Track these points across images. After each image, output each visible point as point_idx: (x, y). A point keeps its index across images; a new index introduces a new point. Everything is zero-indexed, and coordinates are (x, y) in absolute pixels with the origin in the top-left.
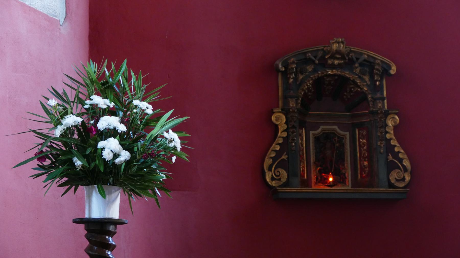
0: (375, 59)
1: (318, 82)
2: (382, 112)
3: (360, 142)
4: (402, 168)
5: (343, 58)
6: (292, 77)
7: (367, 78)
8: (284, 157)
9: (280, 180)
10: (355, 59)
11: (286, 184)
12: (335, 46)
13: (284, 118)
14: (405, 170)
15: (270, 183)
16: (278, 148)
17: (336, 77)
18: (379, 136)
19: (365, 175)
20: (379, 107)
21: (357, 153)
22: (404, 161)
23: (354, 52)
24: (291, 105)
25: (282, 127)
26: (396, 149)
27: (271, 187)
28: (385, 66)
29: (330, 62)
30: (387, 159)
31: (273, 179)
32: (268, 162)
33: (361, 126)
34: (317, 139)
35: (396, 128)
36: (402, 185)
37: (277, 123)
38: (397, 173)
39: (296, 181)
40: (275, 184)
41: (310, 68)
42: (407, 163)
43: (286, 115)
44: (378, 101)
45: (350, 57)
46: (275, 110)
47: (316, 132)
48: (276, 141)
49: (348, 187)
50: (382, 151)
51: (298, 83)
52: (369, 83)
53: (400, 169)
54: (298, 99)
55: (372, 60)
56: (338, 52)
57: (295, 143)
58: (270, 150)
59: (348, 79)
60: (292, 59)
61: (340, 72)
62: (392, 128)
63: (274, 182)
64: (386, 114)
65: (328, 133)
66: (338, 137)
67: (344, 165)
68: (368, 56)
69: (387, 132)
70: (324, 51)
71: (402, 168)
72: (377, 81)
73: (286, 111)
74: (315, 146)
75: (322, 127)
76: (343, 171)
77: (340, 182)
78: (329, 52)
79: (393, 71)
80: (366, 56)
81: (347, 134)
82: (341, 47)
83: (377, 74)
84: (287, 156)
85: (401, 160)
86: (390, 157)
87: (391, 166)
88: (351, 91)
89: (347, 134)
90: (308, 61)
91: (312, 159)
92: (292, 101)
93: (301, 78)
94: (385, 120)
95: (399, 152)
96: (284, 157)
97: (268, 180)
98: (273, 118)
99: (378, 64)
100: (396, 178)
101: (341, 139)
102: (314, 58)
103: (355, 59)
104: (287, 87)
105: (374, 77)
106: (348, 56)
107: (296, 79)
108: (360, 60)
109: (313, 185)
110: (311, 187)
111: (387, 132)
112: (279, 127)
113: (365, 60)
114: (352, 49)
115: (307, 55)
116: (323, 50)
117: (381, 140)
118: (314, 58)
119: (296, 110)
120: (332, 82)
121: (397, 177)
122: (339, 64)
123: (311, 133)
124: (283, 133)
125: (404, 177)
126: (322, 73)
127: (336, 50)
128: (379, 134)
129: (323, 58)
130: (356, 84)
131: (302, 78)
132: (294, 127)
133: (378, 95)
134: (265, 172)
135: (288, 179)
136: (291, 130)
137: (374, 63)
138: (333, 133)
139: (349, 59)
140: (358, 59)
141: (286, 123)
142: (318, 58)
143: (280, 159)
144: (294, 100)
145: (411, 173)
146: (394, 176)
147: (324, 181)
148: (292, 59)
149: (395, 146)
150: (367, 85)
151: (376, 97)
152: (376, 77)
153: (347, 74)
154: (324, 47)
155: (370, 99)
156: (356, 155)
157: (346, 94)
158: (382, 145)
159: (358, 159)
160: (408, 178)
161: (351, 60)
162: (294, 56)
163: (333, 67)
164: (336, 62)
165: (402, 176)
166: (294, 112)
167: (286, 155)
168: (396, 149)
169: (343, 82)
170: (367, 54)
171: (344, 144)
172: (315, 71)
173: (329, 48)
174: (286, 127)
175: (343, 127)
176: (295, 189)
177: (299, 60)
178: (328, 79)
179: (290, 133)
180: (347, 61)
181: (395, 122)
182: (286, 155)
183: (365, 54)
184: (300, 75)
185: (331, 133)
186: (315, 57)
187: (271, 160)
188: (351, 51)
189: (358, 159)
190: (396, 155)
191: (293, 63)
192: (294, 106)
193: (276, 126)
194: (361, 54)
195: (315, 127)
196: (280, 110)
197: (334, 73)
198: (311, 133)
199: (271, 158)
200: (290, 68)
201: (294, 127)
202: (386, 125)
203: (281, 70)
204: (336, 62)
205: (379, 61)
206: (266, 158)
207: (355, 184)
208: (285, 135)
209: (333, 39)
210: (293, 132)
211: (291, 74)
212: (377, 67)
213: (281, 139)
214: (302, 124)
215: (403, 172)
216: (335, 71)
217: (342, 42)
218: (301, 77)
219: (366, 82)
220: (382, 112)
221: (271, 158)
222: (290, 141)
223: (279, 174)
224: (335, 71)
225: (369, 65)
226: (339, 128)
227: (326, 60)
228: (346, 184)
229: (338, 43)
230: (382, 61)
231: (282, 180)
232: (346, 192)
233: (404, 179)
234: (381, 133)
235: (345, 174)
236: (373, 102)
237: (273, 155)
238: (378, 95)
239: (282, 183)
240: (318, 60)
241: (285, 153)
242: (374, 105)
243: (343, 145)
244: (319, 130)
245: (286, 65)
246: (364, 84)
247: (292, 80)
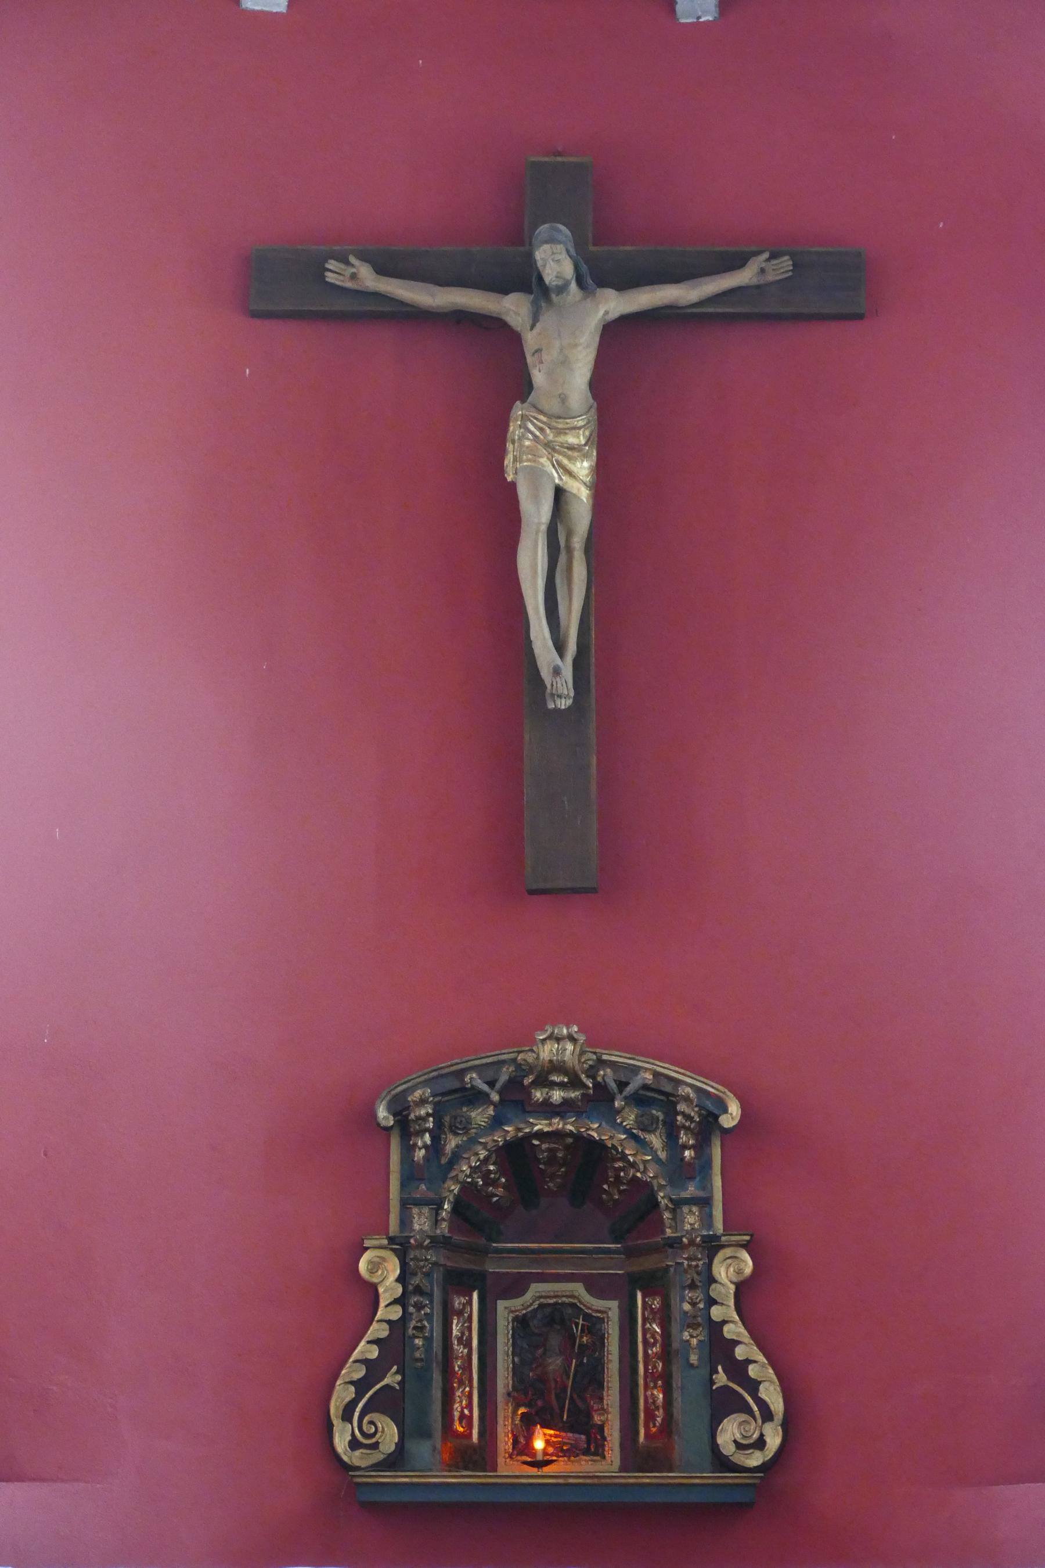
0: (678, 1082)
1: (516, 1155)
2: (692, 1242)
3: (645, 1332)
4: (755, 1408)
5: (575, 1082)
6: (420, 1143)
7: (656, 1141)
8: (392, 1379)
9: (375, 1446)
10: (613, 1086)
11: (395, 1461)
12: (547, 1052)
13: (393, 1268)
14: (767, 1415)
15: (345, 1458)
16: (374, 1353)
17: (570, 1140)
18: (686, 1313)
19: (654, 1430)
20: (688, 1227)
21: (637, 1361)
22: (762, 1388)
23: (612, 1064)
24: (417, 1227)
25: (389, 1287)
26: (740, 1353)
27: (346, 1467)
28: (709, 1105)
29: (538, 1095)
30: (712, 1382)
31: (354, 1444)
32: (342, 1394)
33: (653, 1282)
34: (521, 1323)
35: (743, 1289)
36: (755, 1460)
37: (375, 1280)
38: (740, 1424)
39: (421, 1450)
40: (361, 1458)
41: (480, 1116)
42: (772, 1395)
43: (402, 1256)
44: (685, 1209)
45: (599, 1079)
46: (367, 1243)
47: (517, 1303)
48: (370, 1334)
49: (609, 1465)
50: (694, 1359)
51: (444, 1161)
52: (662, 1155)
53: (749, 1411)
54: (440, 1207)
55: (668, 1088)
56: (557, 1067)
57: (425, 1338)
58: (351, 1360)
59: (600, 1145)
60: (418, 1094)
61: (572, 1124)
62: (732, 1288)
63: (357, 1453)
64: (712, 1246)
65: (556, 1304)
66: (587, 1317)
67: (601, 1399)
68: (656, 1074)
69: (712, 1302)
70: (518, 1066)
71: (755, 1408)
72: (685, 1147)
73: (401, 1247)
74: (514, 1345)
75: (536, 1289)
76: (597, 1419)
77: (586, 1452)
78: (531, 1069)
79: (732, 1115)
80: (649, 1076)
81: (613, 1307)
82: (568, 1052)
83: (687, 1129)
84: (399, 1378)
85: (753, 1386)
86: (721, 1378)
87: (724, 1404)
88: (618, 1180)
89: (613, 1307)
90: (475, 1098)
91: (504, 1380)
92: (420, 1214)
93: (453, 1144)
94: (710, 1265)
95: (748, 1362)
96: (392, 1379)
97: (341, 1443)
98: (363, 1266)
99: (687, 1099)
100: (735, 1441)
101: (594, 1325)
102: (485, 1088)
103: (613, 1086)
104: (411, 1175)
105: (678, 1137)
106: (593, 1077)
107: (435, 1148)
108: (629, 1089)
109: (501, 1460)
110: (496, 1471)
111: (712, 1302)
112: (381, 1290)
113: (645, 1087)
114: (605, 1057)
115: (467, 1079)
116: (514, 1060)
117: (694, 1326)
118: (485, 1088)
119: (427, 1241)
120: (560, 1155)
121: (738, 1436)
122: (566, 1102)
123: (501, 1305)
124: (389, 1308)
125: (762, 1435)
126: (519, 1130)
127: (551, 1061)
128: (687, 1307)
129: (515, 1083)
130: (624, 1157)
131: (457, 1146)
132: (418, 1290)
133: (691, 1190)
134: (332, 1425)
135: (400, 1446)
136: (414, 1299)
137: (673, 1095)
138: (573, 1305)
139: (597, 1085)
140: (622, 1085)
141: (401, 1279)
142: (498, 1086)
143: (378, 1387)
144: (426, 1210)
145: (786, 1425)
146: (730, 1432)
147: (522, 1447)
148: (418, 1094)
149: (736, 1343)
150: (657, 1160)
151: (685, 1195)
152: (683, 1138)
153: (595, 1130)
154: (519, 1052)
155: (664, 1202)
156: (634, 1370)
157: (605, 1187)
158: (694, 1341)
159: (641, 1382)
160: (774, 1440)
161: (600, 1087)
162: (426, 1083)
163: (548, 1109)
164: (557, 1096)
165: (756, 1436)
166: (420, 1246)
167: (397, 1372)
168: (740, 1353)
169: (591, 1157)
170: (648, 1070)
171: (603, 1337)
172: (497, 1122)
173: (530, 1057)
174: (400, 1290)
175: (597, 1286)
176: (432, 1473)
177: (443, 1094)
178: (544, 1146)
179: (411, 1309)
180: (591, 1091)
181: (739, 1272)
182: (397, 1372)
183: (646, 1069)
184: (450, 1136)
185: (563, 1304)
186: (491, 1084)
187: (352, 1389)
188: (601, 1063)
189: (641, 1382)
190: (738, 1370)
191: (423, 1102)
192: (426, 1228)
193: (374, 1288)
194: (635, 1070)
195: (515, 1286)
196: (385, 1242)
197: (555, 1127)
198: (501, 1305)
199: (352, 1383)
200: (412, 1116)
201: (418, 1290)
202: (712, 1280)
203: (384, 1123)
204: (557, 1096)
205: (688, 1090)
206: (338, 1382)
207: (635, 1458)
208: (396, 1313)
209: (543, 1030)
210: (419, 1307)
211: (421, 1133)
212: (681, 1107)
213: (386, 1326)
214: (460, 1281)
215: (760, 1421)
216: (557, 1124)
217: (572, 1038)
218: (452, 1143)
219: (653, 1152)
220: (692, 1242)
221: (352, 1383)
222: (410, 1332)
223: (373, 1430)
224: (557, 1124)
225: (657, 1099)
226: (588, 1290)
227: (526, 1091)
228: (604, 1457)
229: (558, 1040)
230: (698, 1090)
231: (381, 1447)
232: (600, 1485)
233: (760, 1444)
234: (693, 1304)
235: (601, 1428)
236: (673, 1211)
237: (360, 1373)
238: (691, 1190)
239: (381, 1457)
240: (500, 1093)
241: (395, 1367)
242: (674, 1219)
243: (600, 1340)
244: (528, 1296)
245: (401, 1110)
246: (645, 1156)
247: (423, 1151)
